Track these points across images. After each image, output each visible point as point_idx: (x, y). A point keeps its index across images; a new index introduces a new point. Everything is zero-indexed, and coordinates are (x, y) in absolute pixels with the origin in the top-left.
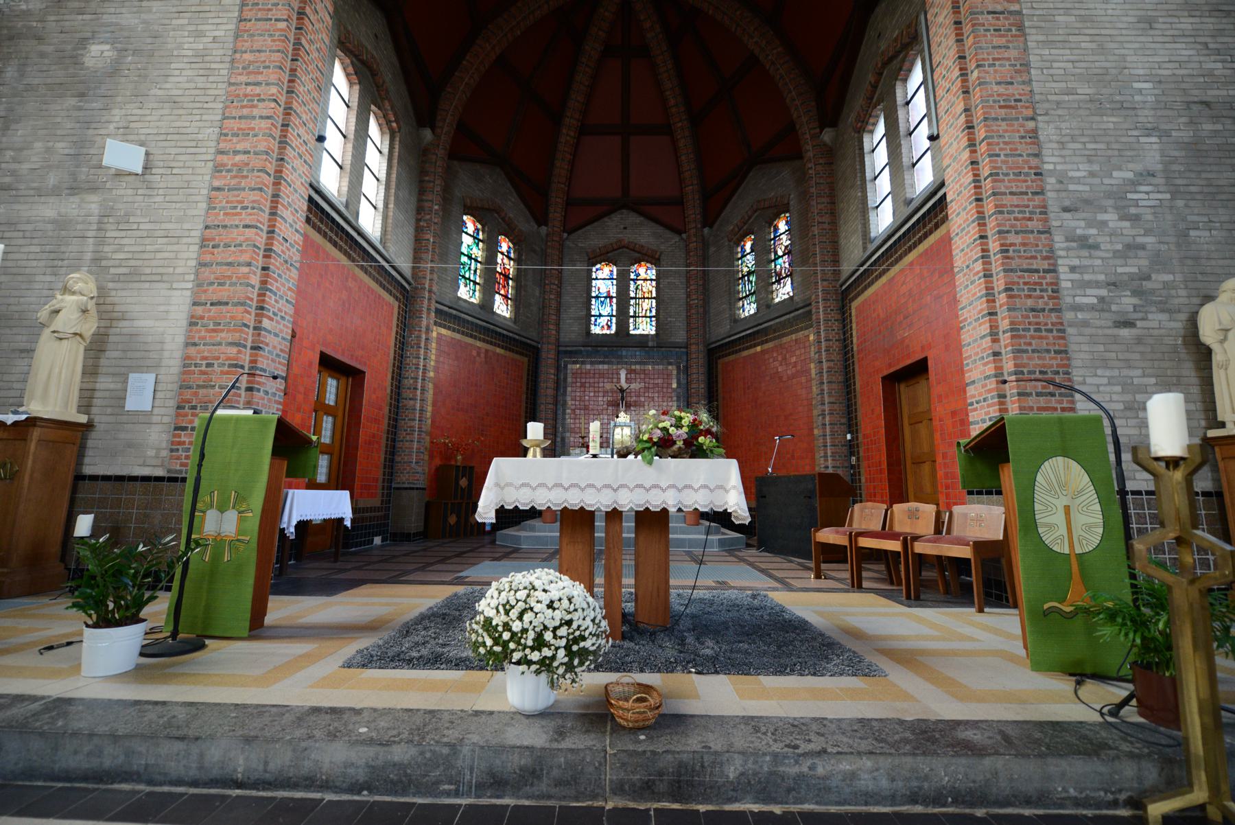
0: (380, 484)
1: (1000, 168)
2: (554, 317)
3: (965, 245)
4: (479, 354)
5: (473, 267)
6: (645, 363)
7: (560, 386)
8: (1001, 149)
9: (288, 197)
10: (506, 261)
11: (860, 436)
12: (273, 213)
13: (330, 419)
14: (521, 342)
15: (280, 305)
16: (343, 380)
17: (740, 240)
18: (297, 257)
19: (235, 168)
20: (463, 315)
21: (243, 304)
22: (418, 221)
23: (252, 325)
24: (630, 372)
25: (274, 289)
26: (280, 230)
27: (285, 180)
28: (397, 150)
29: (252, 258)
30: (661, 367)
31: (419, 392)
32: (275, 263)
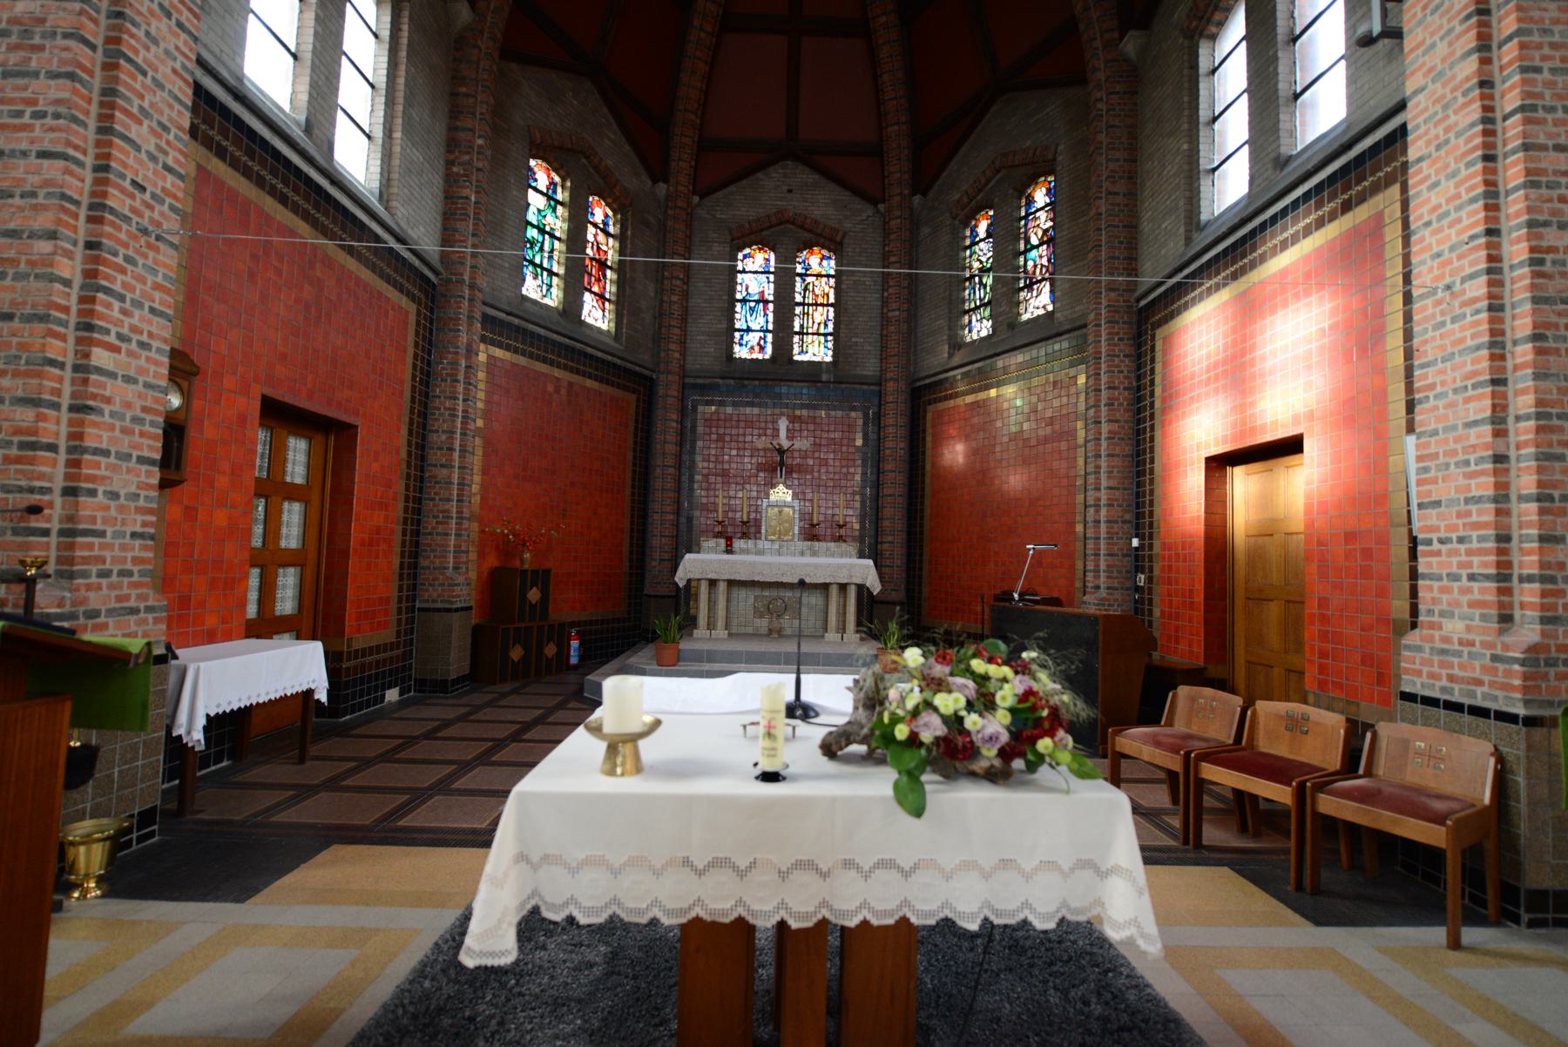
0: (394, 605)
1: (1540, 96)
2: (677, 331)
3: (1445, 247)
4: (557, 390)
5: (547, 247)
6: (815, 407)
7: (685, 439)
8: (1544, 58)
9: (142, 97)
10: (601, 238)
11: (1157, 544)
12: (106, 129)
13: (297, 507)
14: (626, 370)
15: (135, 321)
16: (319, 439)
17: (970, 218)
18: (171, 224)
19: (15, 29)
20: (531, 327)
21: (44, 318)
22: (449, 164)
23: (70, 360)
24: (793, 419)
25: (117, 287)
26: (125, 165)
27: (130, 60)
28: (405, 34)
29: (59, 222)
30: (839, 413)
31: (456, 455)
32: (115, 235)
